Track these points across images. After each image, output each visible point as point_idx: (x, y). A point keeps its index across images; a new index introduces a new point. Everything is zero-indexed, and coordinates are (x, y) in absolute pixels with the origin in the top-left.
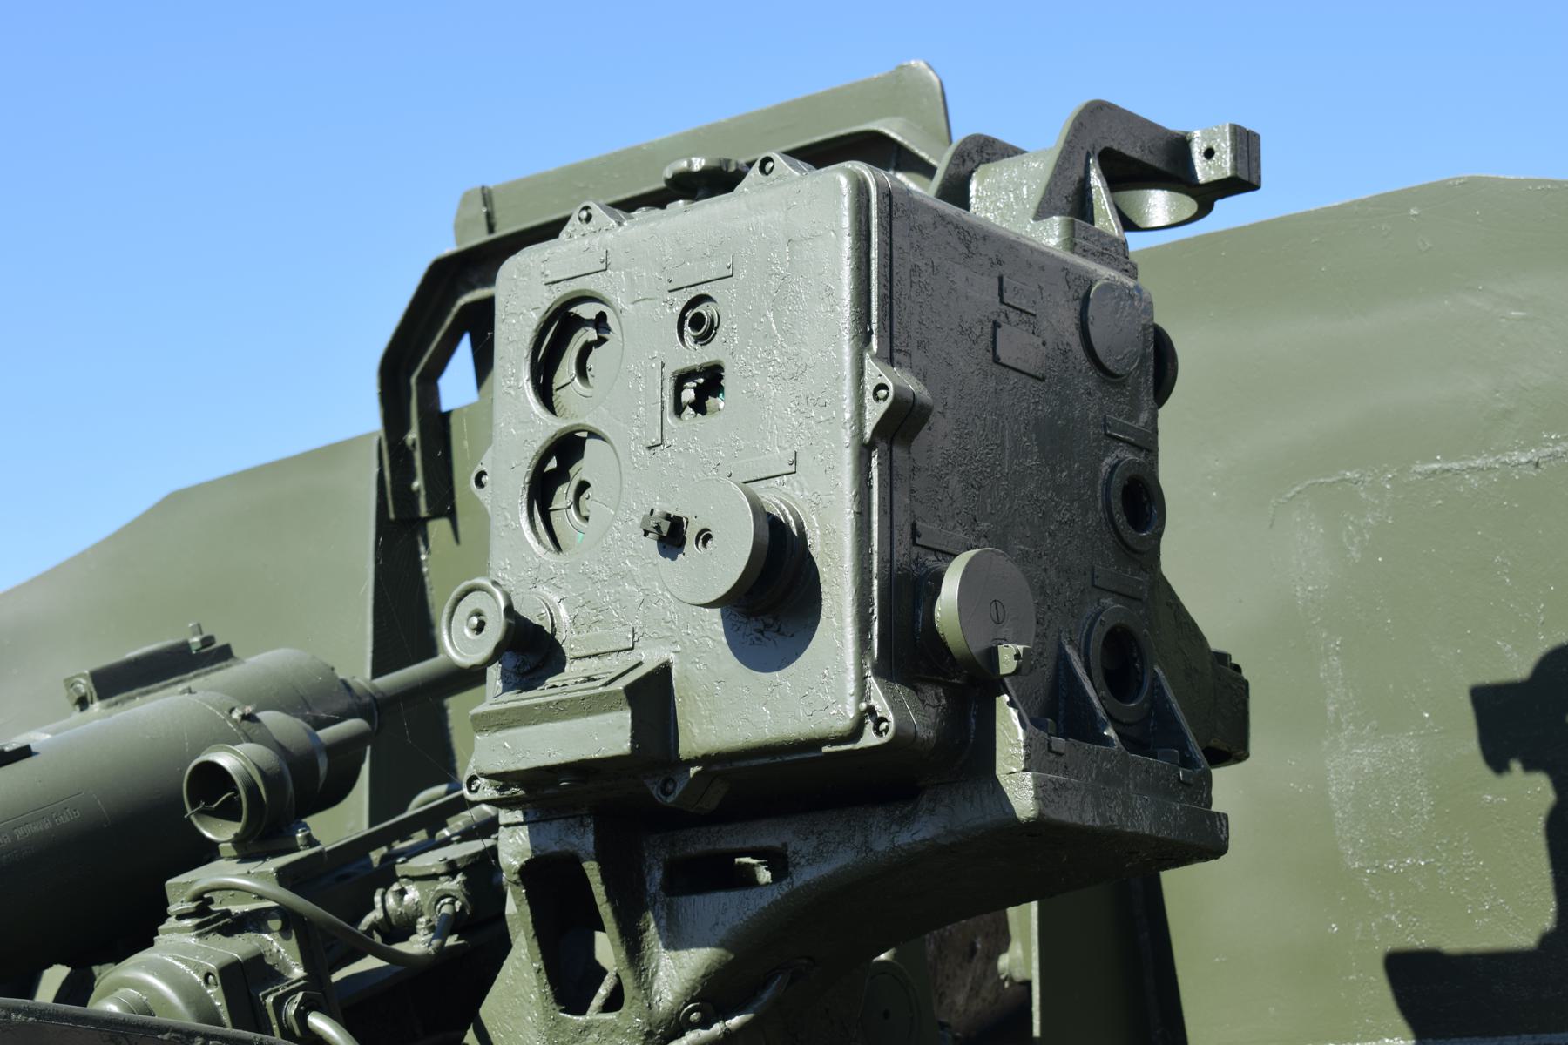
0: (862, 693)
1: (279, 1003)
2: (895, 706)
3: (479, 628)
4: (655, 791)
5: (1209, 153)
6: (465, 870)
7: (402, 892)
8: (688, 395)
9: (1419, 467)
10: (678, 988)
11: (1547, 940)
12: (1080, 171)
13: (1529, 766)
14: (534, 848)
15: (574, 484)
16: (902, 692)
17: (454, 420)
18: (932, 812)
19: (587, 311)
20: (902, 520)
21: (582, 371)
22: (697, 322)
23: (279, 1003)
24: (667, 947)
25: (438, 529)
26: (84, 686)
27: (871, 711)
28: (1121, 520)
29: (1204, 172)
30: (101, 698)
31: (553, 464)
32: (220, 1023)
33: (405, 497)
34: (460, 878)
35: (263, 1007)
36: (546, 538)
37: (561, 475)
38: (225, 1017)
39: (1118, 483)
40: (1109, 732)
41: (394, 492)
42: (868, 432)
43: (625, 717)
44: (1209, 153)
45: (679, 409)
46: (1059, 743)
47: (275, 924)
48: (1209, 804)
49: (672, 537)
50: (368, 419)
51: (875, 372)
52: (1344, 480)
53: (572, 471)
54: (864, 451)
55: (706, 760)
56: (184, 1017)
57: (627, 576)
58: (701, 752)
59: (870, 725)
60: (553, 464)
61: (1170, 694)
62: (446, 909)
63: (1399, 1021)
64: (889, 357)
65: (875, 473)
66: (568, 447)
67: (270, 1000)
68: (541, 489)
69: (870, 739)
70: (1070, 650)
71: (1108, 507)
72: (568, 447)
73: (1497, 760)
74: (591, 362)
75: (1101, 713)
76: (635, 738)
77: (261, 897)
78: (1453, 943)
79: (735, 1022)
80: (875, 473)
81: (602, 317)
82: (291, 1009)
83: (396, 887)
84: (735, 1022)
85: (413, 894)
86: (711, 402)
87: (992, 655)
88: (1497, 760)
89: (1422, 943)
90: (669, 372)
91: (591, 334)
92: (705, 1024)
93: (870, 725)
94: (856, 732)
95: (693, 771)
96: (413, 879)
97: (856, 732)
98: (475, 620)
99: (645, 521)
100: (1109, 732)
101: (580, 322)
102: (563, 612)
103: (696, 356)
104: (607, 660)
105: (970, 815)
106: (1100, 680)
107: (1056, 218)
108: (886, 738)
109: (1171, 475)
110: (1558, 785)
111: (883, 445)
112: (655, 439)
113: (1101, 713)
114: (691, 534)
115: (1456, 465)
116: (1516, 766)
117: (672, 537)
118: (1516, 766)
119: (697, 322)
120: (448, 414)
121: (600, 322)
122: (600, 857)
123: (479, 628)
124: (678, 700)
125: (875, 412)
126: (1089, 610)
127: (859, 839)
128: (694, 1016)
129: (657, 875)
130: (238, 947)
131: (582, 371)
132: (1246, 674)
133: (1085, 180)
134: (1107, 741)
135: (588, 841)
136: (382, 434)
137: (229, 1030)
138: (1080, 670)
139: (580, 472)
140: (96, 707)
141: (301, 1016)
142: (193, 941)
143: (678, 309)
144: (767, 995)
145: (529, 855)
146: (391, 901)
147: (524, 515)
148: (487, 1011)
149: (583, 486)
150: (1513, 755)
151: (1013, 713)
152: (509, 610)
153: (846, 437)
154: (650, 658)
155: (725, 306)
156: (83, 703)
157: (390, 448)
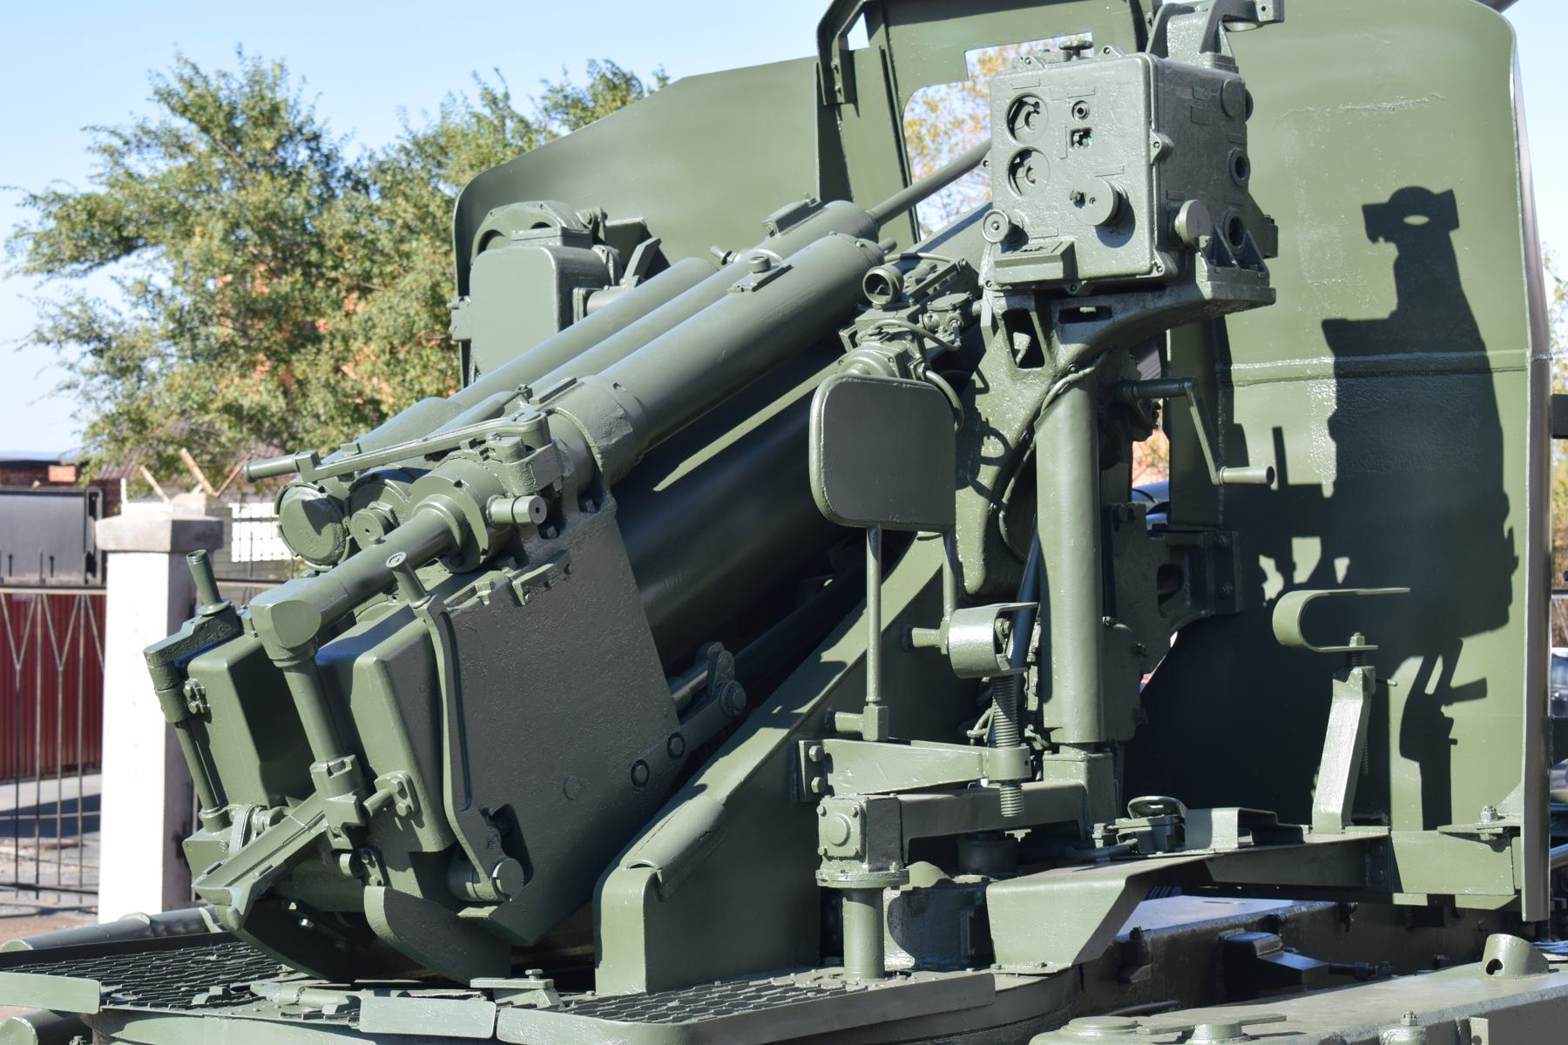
0: (1152, 258)
1: (915, 367)
2: (1165, 262)
3: (997, 228)
4: (1068, 290)
5: (1264, 9)
6: (960, 308)
7: (931, 317)
8: (1076, 138)
9: (1341, 107)
10: (1067, 359)
11: (1393, 315)
12: (1215, 27)
13: (1387, 240)
14: (1008, 306)
15: (1026, 167)
16: (1166, 255)
17: (856, 55)
18: (1171, 295)
19: (1031, 100)
20: (1163, 192)
21: (1027, 122)
22: (1080, 111)
23: (915, 367)
24: (1062, 343)
25: (847, 109)
26: (773, 226)
27: (1156, 264)
28: (1235, 175)
29: (1262, 17)
30: (780, 231)
31: (1018, 160)
32: (895, 376)
33: (831, 93)
34: (958, 311)
35: (909, 369)
36: (1014, 185)
37: (1021, 164)
38: (897, 374)
39: (1234, 160)
40: (1234, 262)
41: (826, 91)
42: (1152, 160)
43: (1060, 264)
44: (1264, 9)
45: (1073, 144)
46: (1219, 269)
47: (910, 337)
48: (1268, 284)
49: (1080, 200)
50: (811, 49)
51: (1154, 137)
52: (1307, 111)
53: (1025, 163)
54: (1150, 166)
55: (1089, 279)
56: (884, 376)
57: (1054, 208)
58: (1087, 276)
59: (1155, 268)
60: (1018, 160)
61: (1253, 242)
62: (954, 325)
63: (1327, 349)
64: (1158, 130)
65: (1154, 175)
66: (1024, 154)
67: (912, 367)
68: (1013, 169)
69: (1155, 274)
70: (1218, 230)
71: (1230, 171)
72: (1024, 154)
73: (1373, 237)
74: (1031, 119)
75: (1230, 254)
76: (1064, 272)
77: (900, 326)
78: (1353, 315)
79: (1087, 370)
80: (1154, 175)
81: (1037, 103)
82: (920, 370)
83: (928, 315)
84: (1087, 370)
85: (935, 317)
86: (1084, 140)
87: (1197, 240)
88: (1373, 237)
89: (1339, 316)
90: (1069, 131)
91: (1032, 109)
92: (1076, 372)
93: (1155, 268)
94: (1150, 271)
95: (1083, 282)
96: (935, 311)
97: (1150, 271)
98: (995, 225)
99: (1071, 195)
100: (1234, 262)
101: (1026, 103)
102: (1027, 219)
103: (1080, 124)
104: (1047, 240)
105: (1184, 296)
106: (1227, 234)
107: (1208, 53)
108: (1161, 274)
109: (1253, 153)
110: (1400, 249)
111: (1156, 164)
112: (1064, 155)
113: (1230, 254)
114: (1087, 199)
115: (1357, 107)
116: (1381, 240)
117: (1080, 200)
118: (1381, 240)
119: (1080, 111)
120: (853, 52)
121: (1036, 105)
122: (1037, 310)
123: (997, 228)
124: (1077, 257)
125: (1154, 152)
126: (1225, 212)
127: (1141, 304)
128: (1073, 369)
129: (1057, 315)
130: (897, 347)
131: (1027, 122)
132: (1276, 223)
133: (1217, 30)
134: (1233, 265)
135: (1032, 304)
136: (819, 61)
137: (899, 379)
138: (1222, 237)
139: (1027, 163)
140: (778, 235)
141: (924, 372)
142: (878, 344)
143: (1072, 105)
144: (1099, 361)
145: (1006, 309)
146: (926, 320)
147: (1008, 186)
148: (982, 366)
149: (1029, 169)
150: (1381, 235)
151: (1203, 260)
152: (1010, 222)
153: (1143, 161)
154: (1067, 240)
155: (1089, 105)
156: (772, 234)
157: (823, 69)
